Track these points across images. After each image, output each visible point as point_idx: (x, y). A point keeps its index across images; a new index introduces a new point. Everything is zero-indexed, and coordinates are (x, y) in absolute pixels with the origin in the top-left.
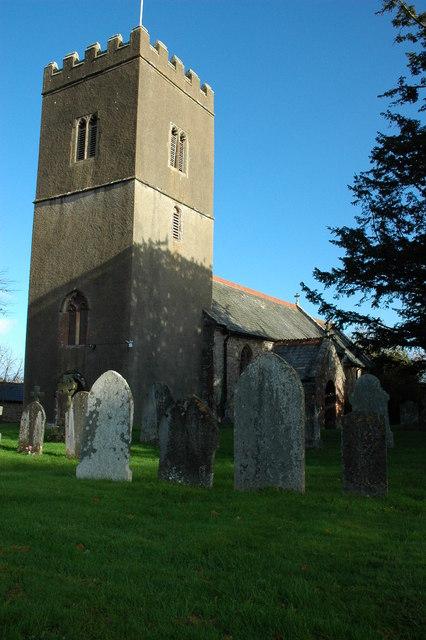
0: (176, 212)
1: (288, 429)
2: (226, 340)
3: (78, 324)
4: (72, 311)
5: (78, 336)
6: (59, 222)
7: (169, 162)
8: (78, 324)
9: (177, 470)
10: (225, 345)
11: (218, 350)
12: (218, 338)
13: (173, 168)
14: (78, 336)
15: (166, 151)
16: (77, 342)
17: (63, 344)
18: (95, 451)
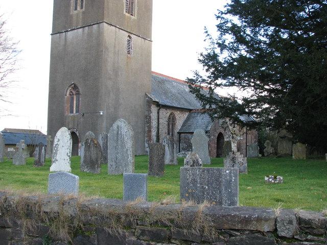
0: (129, 39)
1: (127, 150)
2: (159, 110)
3: (75, 102)
4: (71, 94)
5: (75, 109)
6: (65, 45)
7: (125, 11)
8: (75, 102)
9: (87, 167)
10: (158, 113)
11: (154, 115)
12: (154, 109)
13: (127, 14)
14: (75, 109)
15: (123, 5)
16: (75, 112)
17: (68, 114)
18: (57, 160)
